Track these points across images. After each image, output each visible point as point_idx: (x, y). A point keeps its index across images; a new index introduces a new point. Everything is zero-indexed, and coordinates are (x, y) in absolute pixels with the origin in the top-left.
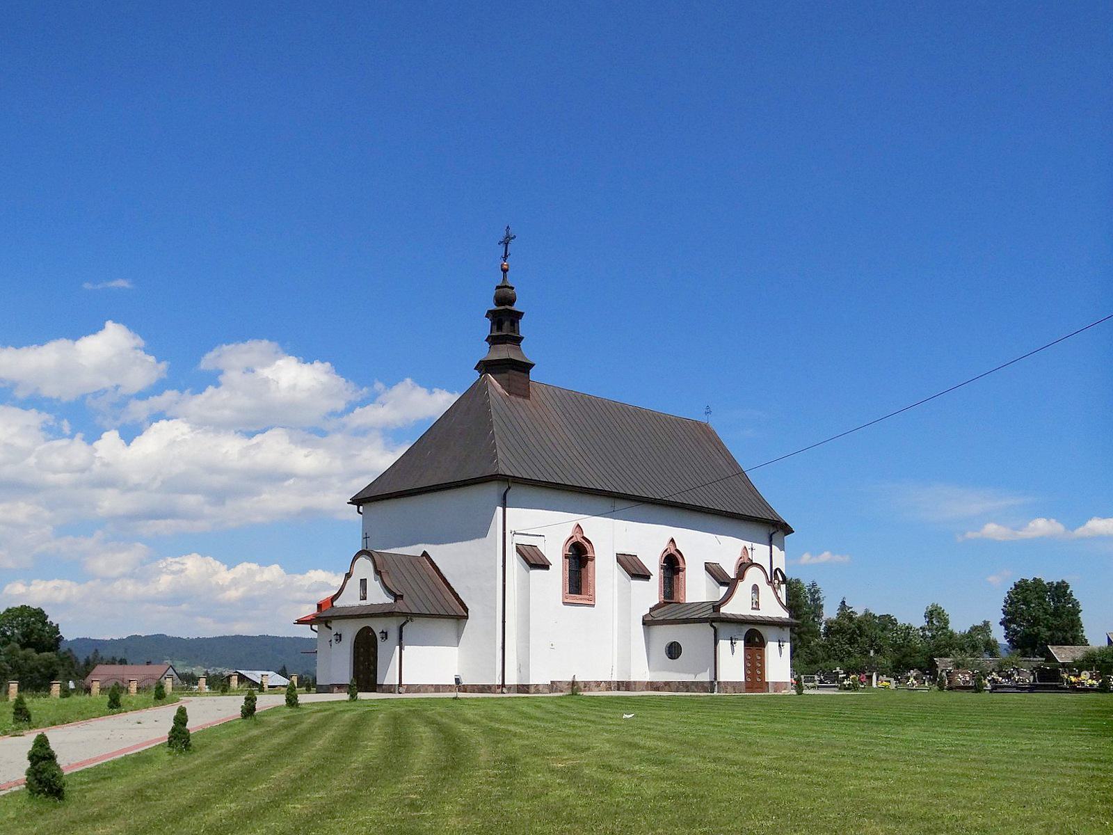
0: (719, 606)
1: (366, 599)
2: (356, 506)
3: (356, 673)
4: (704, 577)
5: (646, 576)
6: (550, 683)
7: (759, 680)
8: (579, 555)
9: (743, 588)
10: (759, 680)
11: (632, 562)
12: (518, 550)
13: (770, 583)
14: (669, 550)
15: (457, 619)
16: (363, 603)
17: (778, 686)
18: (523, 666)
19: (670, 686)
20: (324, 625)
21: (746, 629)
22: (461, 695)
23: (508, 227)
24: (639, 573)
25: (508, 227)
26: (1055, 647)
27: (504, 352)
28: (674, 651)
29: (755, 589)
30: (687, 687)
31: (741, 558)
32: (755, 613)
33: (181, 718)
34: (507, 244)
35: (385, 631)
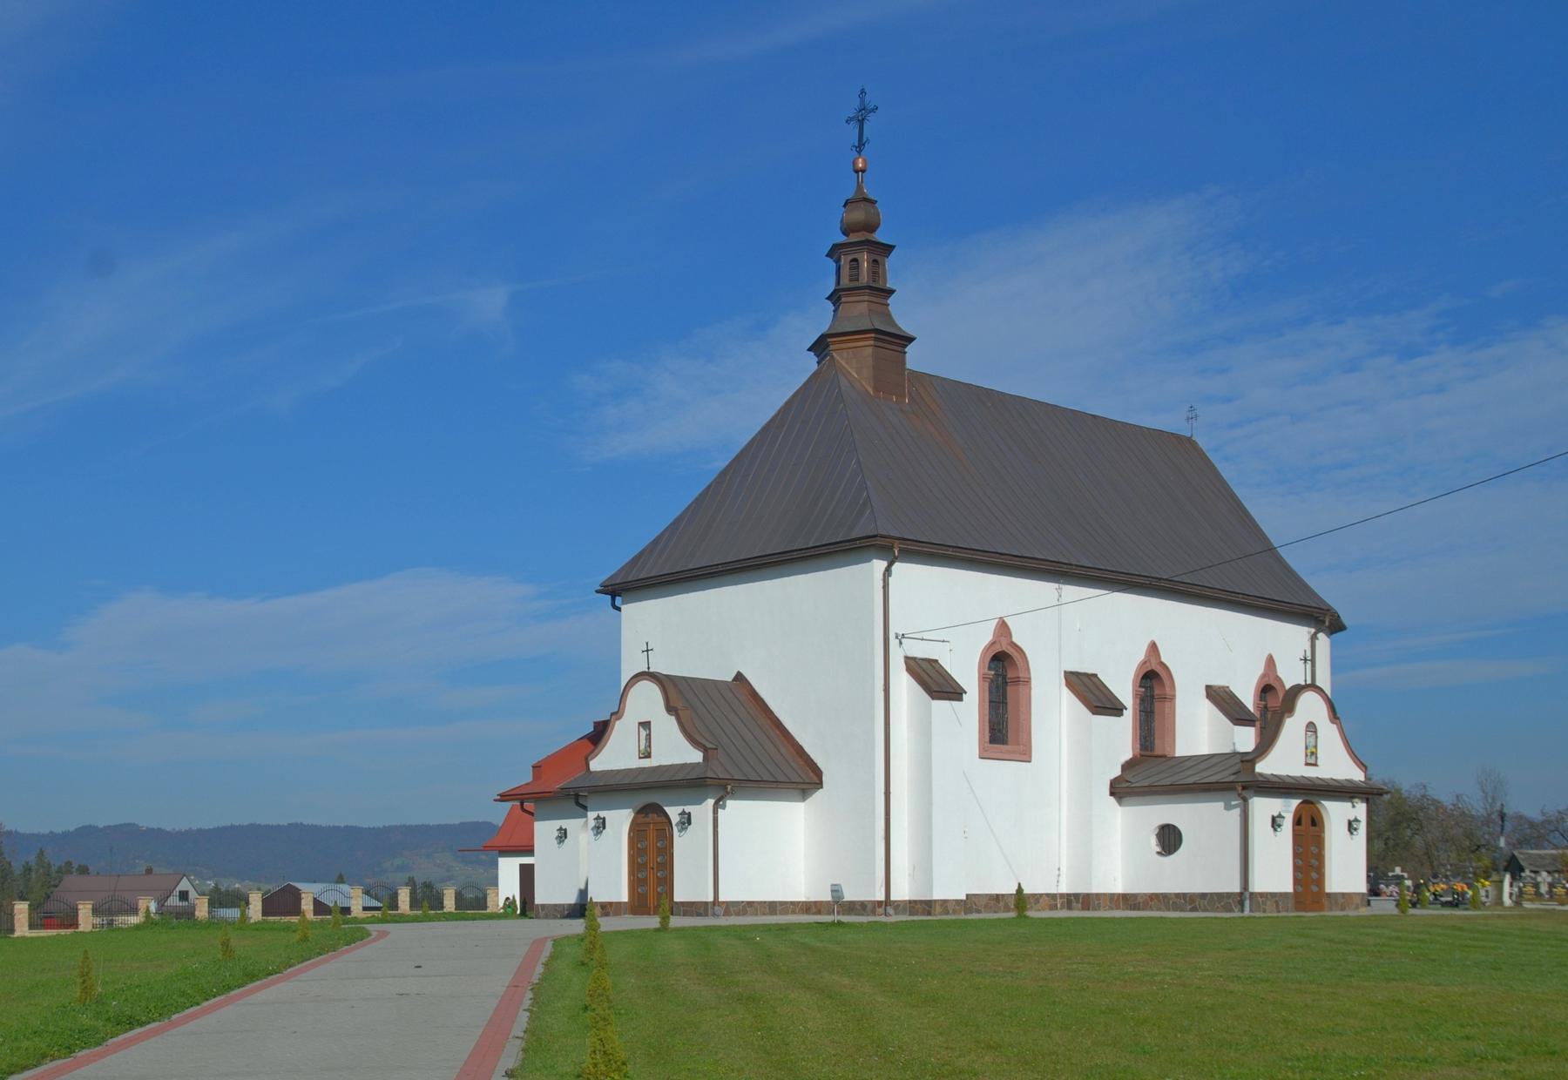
3: (635, 882)
4: (1207, 710)
5: (954, 693)
6: (964, 898)
7: (1314, 888)
9: (1292, 729)
10: (1314, 888)
11: (933, 674)
12: (909, 670)
14: (1148, 664)
16: (646, 763)
17: (1345, 899)
18: (924, 867)
20: (573, 802)
22: (845, 919)
23: (863, 91)
24: (1108, 706)
25: (863, 91)
27: (859, 312)
28: (1169, 839)
29: (1311, 727)
31: (1146, 662)
32: (1311, 773)
34: (861, 123)
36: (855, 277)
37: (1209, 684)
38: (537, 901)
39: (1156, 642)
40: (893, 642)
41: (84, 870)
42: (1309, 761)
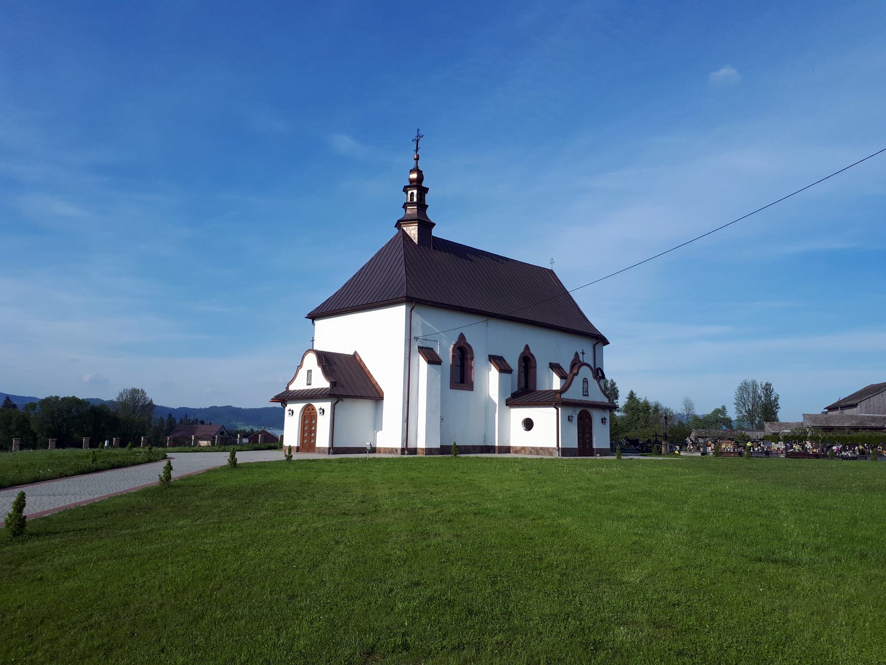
0: (168, 478)
1: (310, 385)
2: (311, 320)
3: (302, 438)
8: (463, 353)
9: (577, 382)
13: (595, 378)
15: (376, 400)
19: (525, 450)
21: (578, 410)
23: (418, 130)
25: (418, 130)
26: (768, 423)
28: (528, 424)
29: (585, 381)
30: (537, 451)
32: (584, 399)
33: (20, 504)
34: (418, 141)
35: (291, 409)
36: (412, 199)
37: (551, 362)
38: (595, 446)
39: (529, 345)
40: (413, 340)
41: (203, 423)
42: (585, 394)
